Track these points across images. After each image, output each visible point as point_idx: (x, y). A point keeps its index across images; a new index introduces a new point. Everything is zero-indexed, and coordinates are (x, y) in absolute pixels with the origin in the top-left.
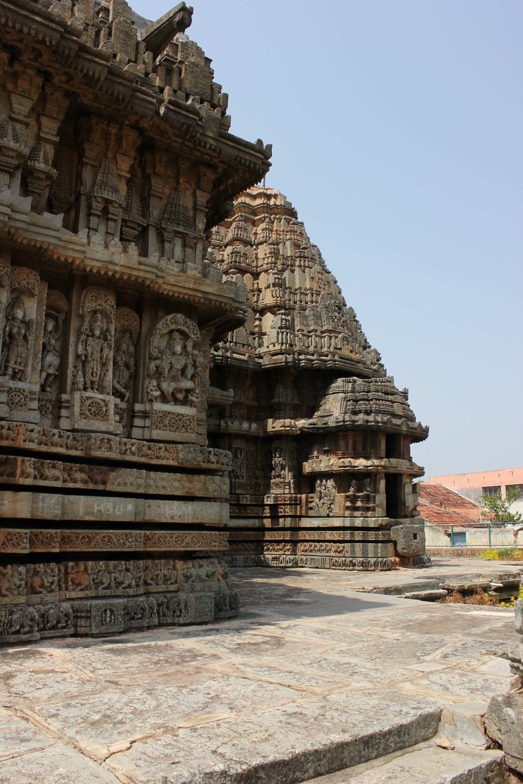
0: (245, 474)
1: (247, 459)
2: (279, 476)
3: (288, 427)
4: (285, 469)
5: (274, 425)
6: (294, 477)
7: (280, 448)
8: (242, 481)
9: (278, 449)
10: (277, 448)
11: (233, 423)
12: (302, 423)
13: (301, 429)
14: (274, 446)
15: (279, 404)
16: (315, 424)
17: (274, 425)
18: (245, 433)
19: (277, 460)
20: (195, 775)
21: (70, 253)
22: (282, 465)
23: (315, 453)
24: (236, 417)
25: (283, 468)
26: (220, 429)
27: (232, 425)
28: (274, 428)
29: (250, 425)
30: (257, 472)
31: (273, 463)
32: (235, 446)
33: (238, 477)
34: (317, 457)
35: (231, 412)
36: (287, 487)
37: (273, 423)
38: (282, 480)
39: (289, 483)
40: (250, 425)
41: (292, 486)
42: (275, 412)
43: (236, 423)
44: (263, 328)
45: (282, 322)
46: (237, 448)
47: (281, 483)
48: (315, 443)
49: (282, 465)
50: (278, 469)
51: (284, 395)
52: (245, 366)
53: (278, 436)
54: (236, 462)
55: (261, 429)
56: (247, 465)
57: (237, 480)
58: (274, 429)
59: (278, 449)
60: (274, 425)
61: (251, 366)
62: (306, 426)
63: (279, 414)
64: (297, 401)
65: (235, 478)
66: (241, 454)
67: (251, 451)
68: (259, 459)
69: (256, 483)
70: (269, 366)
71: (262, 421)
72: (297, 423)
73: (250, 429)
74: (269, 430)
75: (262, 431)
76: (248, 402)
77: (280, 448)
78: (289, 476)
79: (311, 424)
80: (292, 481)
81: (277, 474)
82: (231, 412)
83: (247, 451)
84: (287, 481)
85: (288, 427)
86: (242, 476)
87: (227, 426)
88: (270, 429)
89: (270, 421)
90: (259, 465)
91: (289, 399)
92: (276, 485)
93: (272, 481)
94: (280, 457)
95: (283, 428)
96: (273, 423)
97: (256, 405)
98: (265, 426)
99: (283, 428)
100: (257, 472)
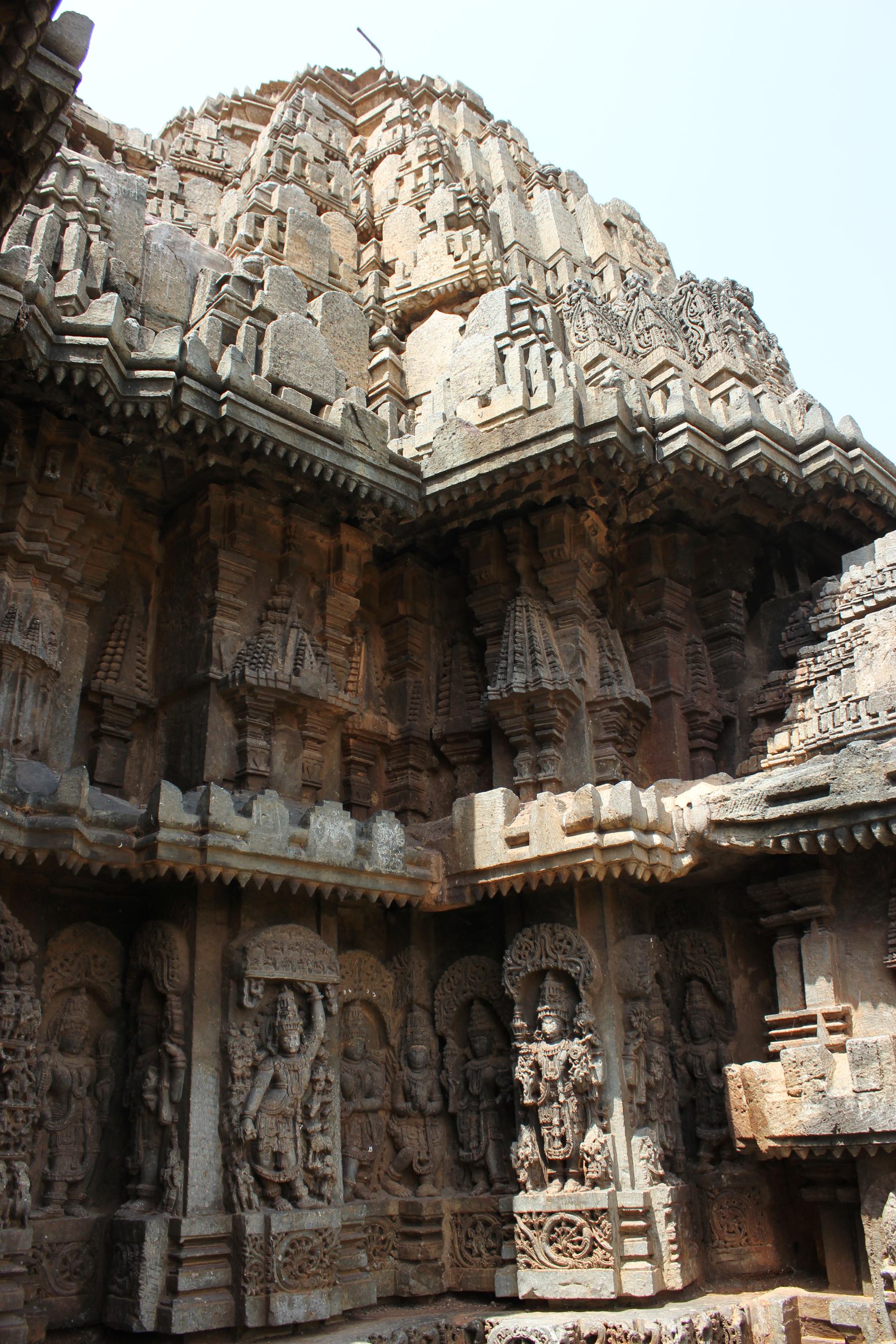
0: (333, 1165)
1: (347, 1055)
2: (569, 1168)
3: (624, 824)
4: (603, 1117)
5: (514, 828)
6: (670, 1165)
7: (562, 976)
8: (312, 1219)
9: (550, 984)
10: (541, 974)
11: (246, 812)
12: (696, 803)
13: (698, 842)
14: (519, 960)
15: (533, 702)
16: (823, 790)
17: (518, 826)
18: (330, 878)
19: (546, 1055)
20: (322, 1131)
21: (236, 862)
22: (582, 1090)
23: (820, 996)
24: (267, 782)
25: (591, 1107)
26: (149, 849)
27: (240, 823)
28: (518, 841)
29: (364, 834)
30: (412, 1136)
31: (523, 1073)
32: (261, 969)
33: (288, 1190)
34: (841, 1021)
35: (242, 753)
36: (637, 1246)
37: (512, 813)
38: (598, 1198)
39: (646, 1213)
40: (364, 834)
41: (666, 1231)
42: (504, 745)
43: (271, 812)
44: (410, 379)
45: (511, 318)
46: (276, 986)
47: (593, 1215)
48: (800, 929)
49: (582, 1090)
50: (560, 1115)
51: (554, 652)
52: (329, 456)
53: (545, 897)
54: (275, 1083)
55: (436, 858)
56: (346, 1095)
57: (281, 1222)
58: (524, 853)
59: (550, 984)
60: (514, 828)
61: (361, 470)
62: (742, 813)
63: (537, 767)
64: (628, 688)
65: (268, 1201)
66: (309, 1025)
67: (368, 1003)
68: (420, 1051)
69: (411, 1216)
70: (471, 474)
71: (433, 813)
72: (669, 803)
73: (363, 852)
74: (483, 861)
75: (436, 869)
76: (344, 700)
77: (562, 976)
78: (631, 1163)
79: (775, 799)
80: (662, 1195)
81: (556, 1152)
82: (242, 753)
83: (346, 1006)
84: (630, 1199)
85: (624, 824)
86: (318, 1180)
87: (205, 827)
88: (490, 850)
89: (490, 805)
90: (422, 1093)
91: (591, 676)
92: (559, 1229)
93: (523, 1203)
94: (569, 1030)
95: (589, 838)
96: (512, 813)
97: (392, 730)
98: (457, 843)
99: (589, 838)
100: (412, 1136)
